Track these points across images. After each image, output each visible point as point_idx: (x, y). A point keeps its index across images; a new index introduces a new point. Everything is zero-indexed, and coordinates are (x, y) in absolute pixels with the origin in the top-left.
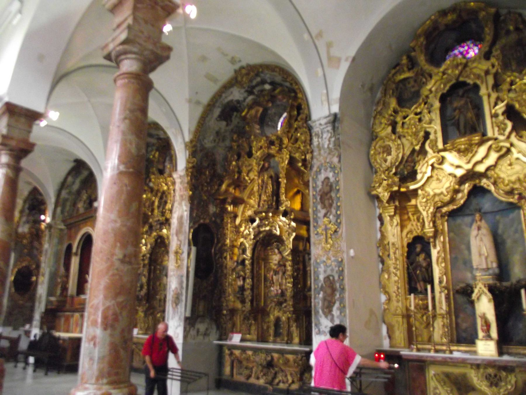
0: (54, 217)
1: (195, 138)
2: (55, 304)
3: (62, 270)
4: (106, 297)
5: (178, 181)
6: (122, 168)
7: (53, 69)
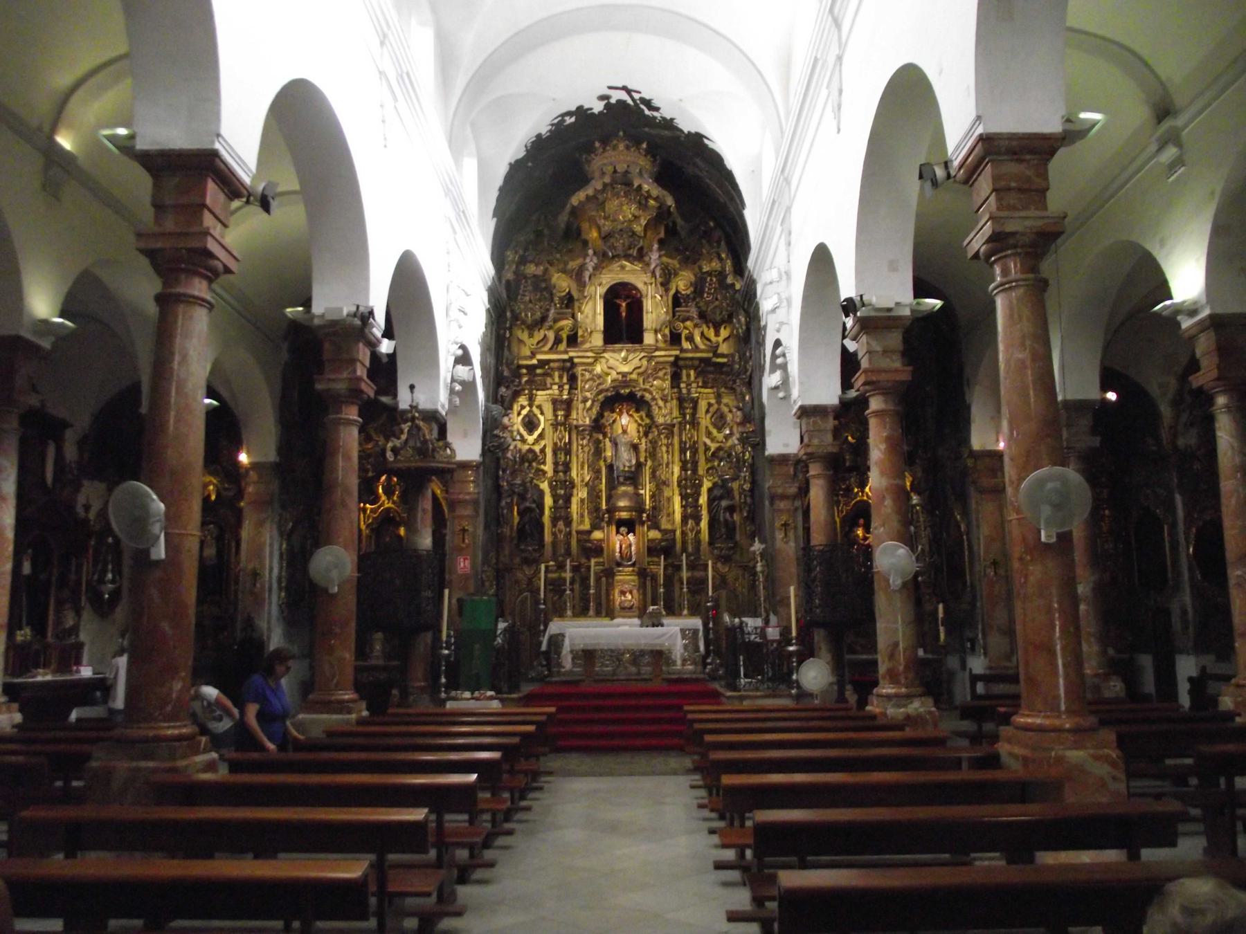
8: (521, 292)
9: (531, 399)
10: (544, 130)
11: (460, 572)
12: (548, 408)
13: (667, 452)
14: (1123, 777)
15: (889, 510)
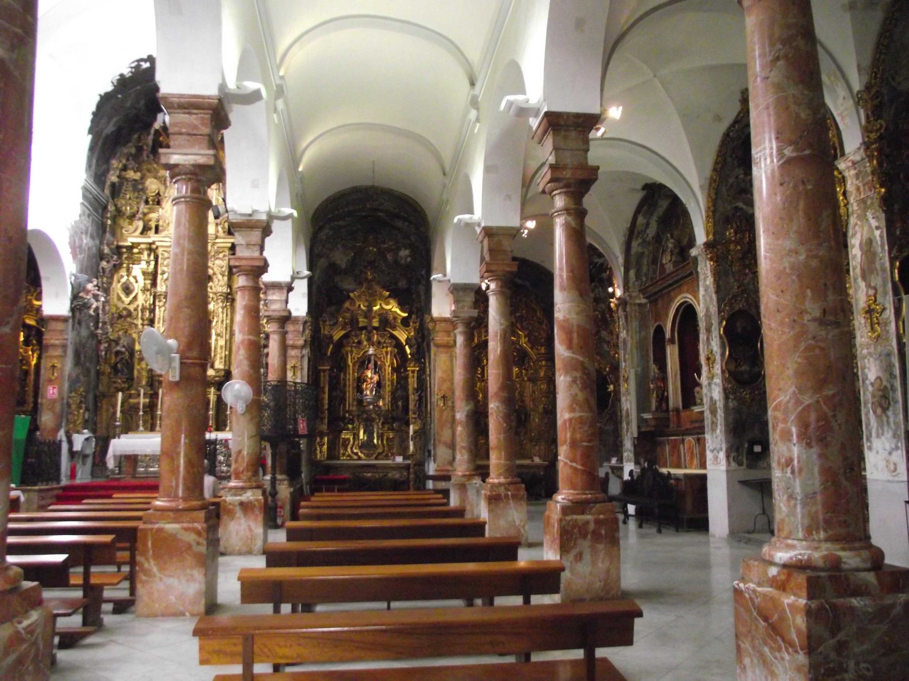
0: (626, 287)
1: (876, 78)
2: (653, 423)
3: (653, 368)
4: (801, 390)
5: (850, 174)
6: (788, 152)
7: (600, 36)
8: (123, 191)
9: (129, 271)
10: (127, 72)
11: (49, 397)
12: (141, 278)
13: (223, 312)
14: (205, 542)
15: (241, 357)
